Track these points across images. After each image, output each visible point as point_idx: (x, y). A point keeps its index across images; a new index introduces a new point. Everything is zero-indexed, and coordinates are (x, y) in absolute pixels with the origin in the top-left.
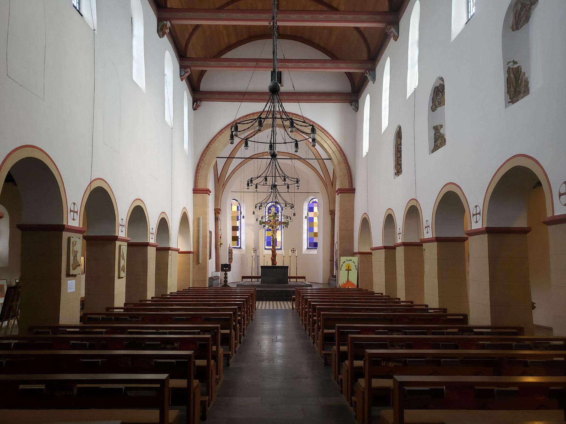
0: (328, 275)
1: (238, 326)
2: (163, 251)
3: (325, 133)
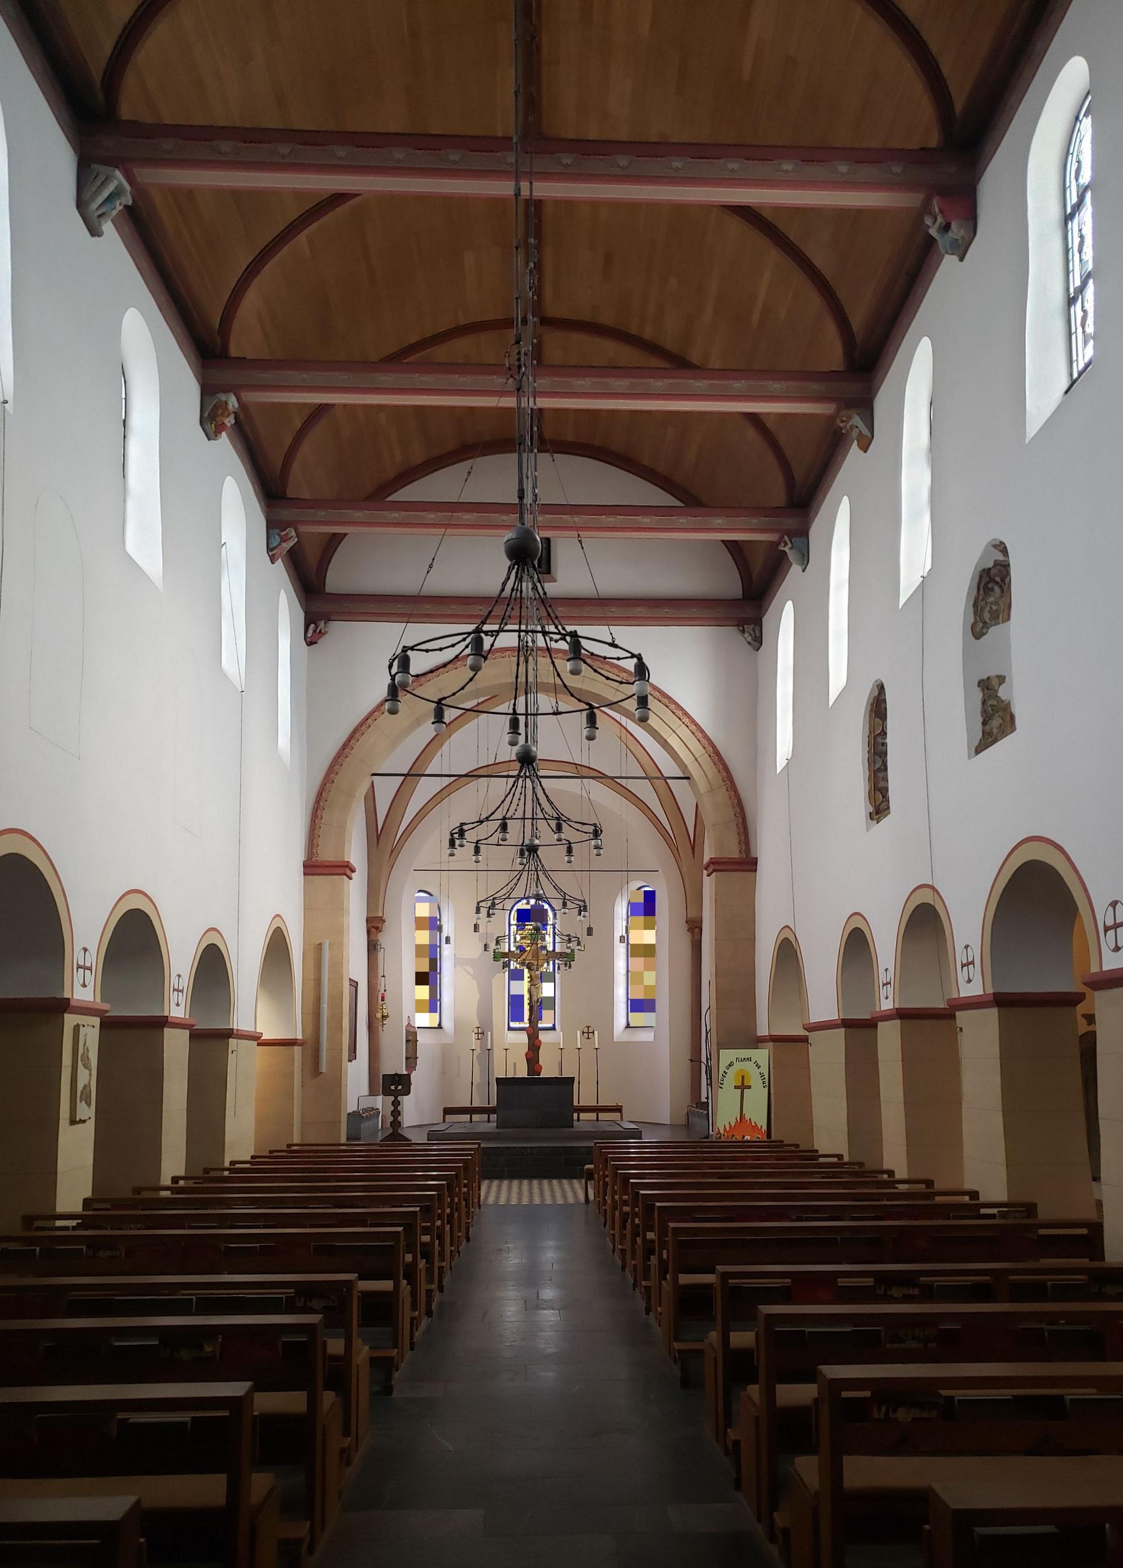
0: (686, 1100)
1: (422, 1264)
2: (212, 1041)
3: (673, 706)
